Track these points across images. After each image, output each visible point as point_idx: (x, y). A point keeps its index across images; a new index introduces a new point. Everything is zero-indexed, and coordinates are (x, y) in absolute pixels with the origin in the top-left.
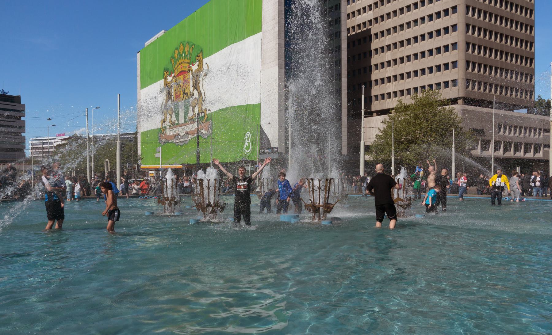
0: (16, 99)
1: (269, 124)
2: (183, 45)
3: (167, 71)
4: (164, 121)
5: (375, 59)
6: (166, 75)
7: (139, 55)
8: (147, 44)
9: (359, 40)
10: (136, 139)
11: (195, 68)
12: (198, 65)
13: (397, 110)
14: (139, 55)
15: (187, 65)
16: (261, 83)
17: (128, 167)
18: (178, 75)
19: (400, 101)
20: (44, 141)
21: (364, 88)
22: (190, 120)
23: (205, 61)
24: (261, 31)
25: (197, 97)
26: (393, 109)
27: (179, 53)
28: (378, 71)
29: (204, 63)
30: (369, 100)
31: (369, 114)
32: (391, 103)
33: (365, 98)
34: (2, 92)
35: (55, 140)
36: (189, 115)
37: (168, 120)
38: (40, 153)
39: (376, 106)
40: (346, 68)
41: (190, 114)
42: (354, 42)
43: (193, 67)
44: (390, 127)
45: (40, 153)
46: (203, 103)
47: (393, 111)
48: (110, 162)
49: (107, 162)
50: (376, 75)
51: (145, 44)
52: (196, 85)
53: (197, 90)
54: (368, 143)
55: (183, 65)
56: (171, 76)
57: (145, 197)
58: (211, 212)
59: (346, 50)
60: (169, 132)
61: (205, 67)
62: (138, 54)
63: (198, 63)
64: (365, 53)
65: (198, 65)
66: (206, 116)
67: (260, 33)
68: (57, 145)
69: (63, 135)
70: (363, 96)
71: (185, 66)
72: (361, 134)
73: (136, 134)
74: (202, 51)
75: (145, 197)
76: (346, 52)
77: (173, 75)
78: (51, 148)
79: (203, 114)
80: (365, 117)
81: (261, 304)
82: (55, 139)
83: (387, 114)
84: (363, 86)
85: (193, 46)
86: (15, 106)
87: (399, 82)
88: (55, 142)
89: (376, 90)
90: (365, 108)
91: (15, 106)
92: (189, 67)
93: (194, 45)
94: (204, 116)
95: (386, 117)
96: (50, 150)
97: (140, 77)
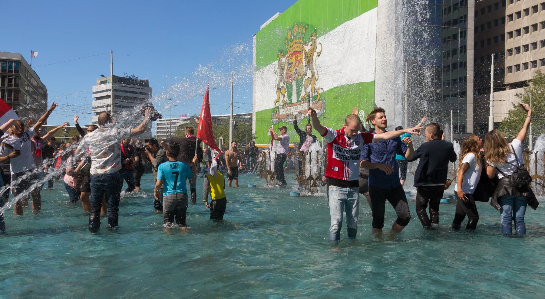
0: (144, 84)
1: (384, 100)
2: (298, 25)
3: (282, 53)
4: (277, 101)
5: (510, 26)
6: (280, 56)
7: (254, 37)
8: (262, 27)
9: (490, 7)
10: (251, 119)
11: (308, 48)
12: (312, 45)
13: (535, 81)
14: (254, 37)
15: (300, 45)
16: (375, 60)
17: (243, 145)
18: (292, 55)
19: (538, 72)
20: (168, 122)
21: (495, 57)
22: (303, 99)
23: (318, 41)
24: (377, 6)
25: (310, 77)
26: (530, 81)
27: (292, 34)
28: (512, 39)
29: (318, 43)
30: (500, 74)
31: (500, 87)
32: (527, 75)
33: (495, 70)
34: (133, 77)
35: (178, 121)
36: (301, 95)
37: (281, 101)
38: (164, 132)
39: (509, 78)
40: (473, 38)
41: (303, 94)
42: (483, 11)
43: (305, 47)
44: (527, 101)
45: (164, 132)
46: (316, 82)
47: (531, 84)
48: (224, 140)
49: (221, 139)
50: (509, 44)
51: (261, 27)
52: (309, 63)
53: (310, 70)
54: (499, 120)
55: (296, 45)
56: (285, 57)
57: (253, 172)
58: (312, 185)
59: (473, 19)
60: (282, 112)
61: (319, 47)
62: (254, 37)
63: (311, 43)
64: (496, 22)
65: (312, 45)
66: (319, 96)
67: (376, 8)
68: (180, 125)
69: (185, 116)
70: (492, 66)
71: (298, 46)
72: (489, 108)
73: (251, 114)
74: (315, 30)
75: (253, 172)
76: (474, 21)
77: (287, 56)
78: (174, 128)
79: (316, 93)
80: (494, 92)
81: (54, 128)
82: (178, 119)
83: (522, 87)
84: (493, 55)
85: (307, 26)
86: (144, 89)
87: (514, 39)
88: (178, 122)
89: (509, 61)
90: (494, 79)
91: (144, 89)
92: (303, 47)
93: (308, 25)
94: (317, 96)
95: (520, 90)
96: (172, 130)
97: (255, 59)
